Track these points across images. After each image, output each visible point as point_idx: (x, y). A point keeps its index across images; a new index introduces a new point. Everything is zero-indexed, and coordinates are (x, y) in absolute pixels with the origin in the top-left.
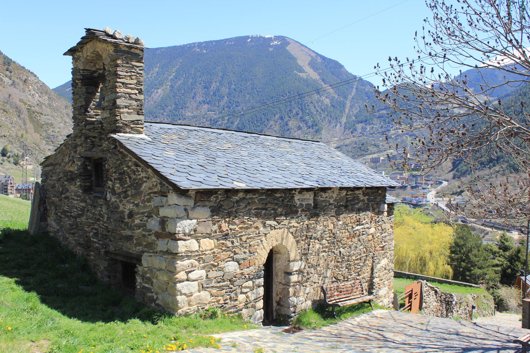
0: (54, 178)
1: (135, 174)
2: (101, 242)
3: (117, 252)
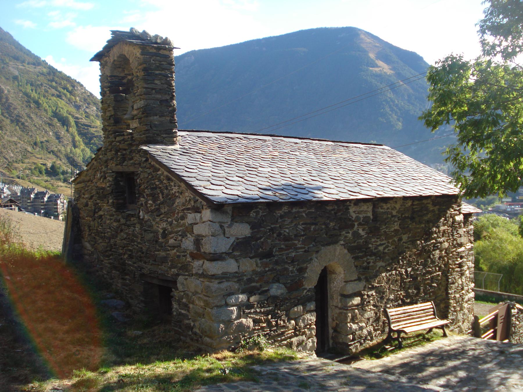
0: (86, 196)
1: (167, 189)
2: (135, 265)
3: (152, 275)
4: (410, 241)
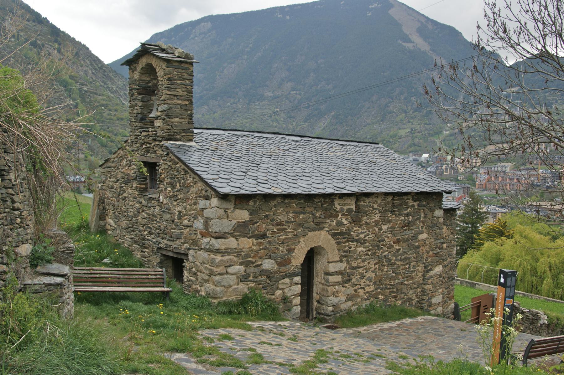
4: (389, 231)
